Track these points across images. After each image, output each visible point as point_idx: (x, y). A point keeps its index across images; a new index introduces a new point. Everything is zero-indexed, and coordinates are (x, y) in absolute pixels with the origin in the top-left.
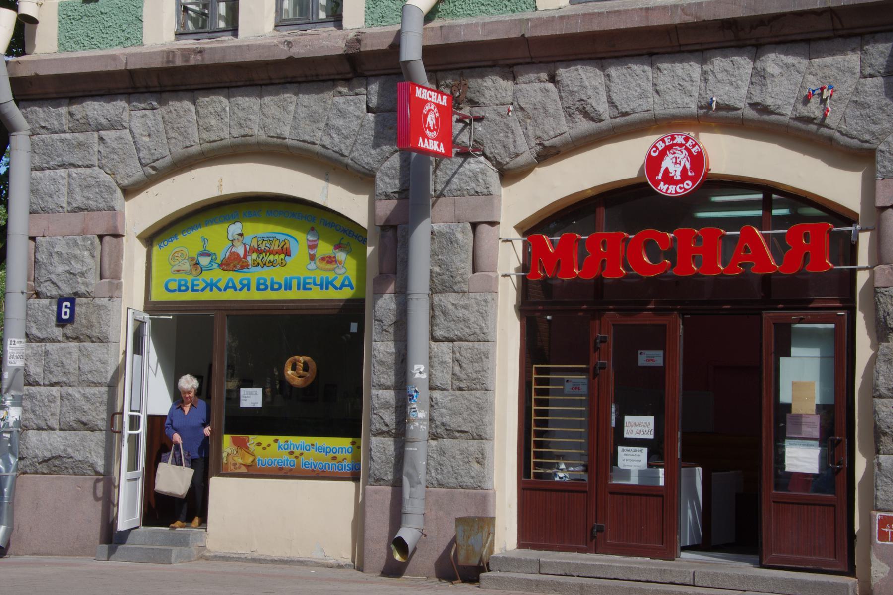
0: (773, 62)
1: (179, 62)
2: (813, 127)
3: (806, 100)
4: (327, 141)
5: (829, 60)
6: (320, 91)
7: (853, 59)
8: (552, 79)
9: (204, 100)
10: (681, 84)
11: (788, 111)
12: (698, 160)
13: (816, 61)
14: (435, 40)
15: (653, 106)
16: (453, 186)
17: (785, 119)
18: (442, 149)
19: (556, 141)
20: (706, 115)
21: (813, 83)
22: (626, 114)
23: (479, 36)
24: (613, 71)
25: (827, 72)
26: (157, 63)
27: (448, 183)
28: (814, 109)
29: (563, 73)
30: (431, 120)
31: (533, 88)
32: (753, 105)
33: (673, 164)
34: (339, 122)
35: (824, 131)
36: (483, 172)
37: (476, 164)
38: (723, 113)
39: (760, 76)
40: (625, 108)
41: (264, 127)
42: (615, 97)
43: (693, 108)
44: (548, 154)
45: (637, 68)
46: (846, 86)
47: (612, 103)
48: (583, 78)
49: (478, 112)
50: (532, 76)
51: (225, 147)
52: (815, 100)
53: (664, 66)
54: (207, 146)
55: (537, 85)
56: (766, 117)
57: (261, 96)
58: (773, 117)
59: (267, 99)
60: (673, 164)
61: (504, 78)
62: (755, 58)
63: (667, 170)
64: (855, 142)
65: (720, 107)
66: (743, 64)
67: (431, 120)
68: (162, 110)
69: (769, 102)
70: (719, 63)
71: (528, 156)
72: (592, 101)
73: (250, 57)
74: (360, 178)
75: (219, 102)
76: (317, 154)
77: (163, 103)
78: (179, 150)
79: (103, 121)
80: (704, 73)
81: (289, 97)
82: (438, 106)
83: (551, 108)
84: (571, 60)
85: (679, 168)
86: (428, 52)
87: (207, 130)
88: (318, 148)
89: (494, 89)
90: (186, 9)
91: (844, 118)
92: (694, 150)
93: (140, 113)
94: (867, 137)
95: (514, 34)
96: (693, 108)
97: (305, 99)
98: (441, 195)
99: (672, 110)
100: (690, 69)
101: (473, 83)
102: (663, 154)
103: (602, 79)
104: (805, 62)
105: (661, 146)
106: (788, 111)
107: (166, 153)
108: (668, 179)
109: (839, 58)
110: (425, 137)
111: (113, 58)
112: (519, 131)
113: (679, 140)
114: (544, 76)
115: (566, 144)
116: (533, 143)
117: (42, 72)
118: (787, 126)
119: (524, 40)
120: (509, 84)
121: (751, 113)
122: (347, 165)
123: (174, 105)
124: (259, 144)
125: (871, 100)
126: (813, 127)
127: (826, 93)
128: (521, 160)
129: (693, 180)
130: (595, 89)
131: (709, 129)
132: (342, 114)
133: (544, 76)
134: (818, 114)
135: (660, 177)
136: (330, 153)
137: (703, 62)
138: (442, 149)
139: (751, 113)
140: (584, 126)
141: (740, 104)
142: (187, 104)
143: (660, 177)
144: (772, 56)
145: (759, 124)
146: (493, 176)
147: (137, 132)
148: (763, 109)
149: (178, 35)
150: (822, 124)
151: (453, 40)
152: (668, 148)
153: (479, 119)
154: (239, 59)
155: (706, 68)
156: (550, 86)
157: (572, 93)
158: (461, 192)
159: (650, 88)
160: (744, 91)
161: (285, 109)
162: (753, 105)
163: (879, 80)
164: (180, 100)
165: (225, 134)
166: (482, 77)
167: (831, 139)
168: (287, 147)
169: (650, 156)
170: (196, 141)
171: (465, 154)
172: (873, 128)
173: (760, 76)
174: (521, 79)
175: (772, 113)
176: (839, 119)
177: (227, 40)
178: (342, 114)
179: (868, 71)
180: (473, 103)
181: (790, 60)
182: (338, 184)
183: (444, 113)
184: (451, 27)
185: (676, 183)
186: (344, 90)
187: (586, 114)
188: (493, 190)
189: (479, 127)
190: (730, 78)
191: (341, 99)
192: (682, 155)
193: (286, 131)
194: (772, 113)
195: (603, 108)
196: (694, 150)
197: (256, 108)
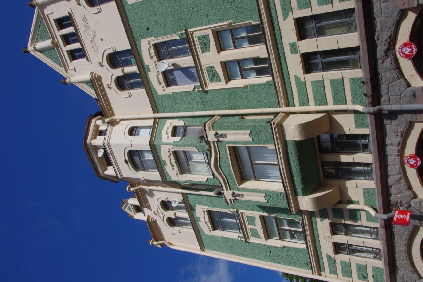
0: (388, 142)
1: (387, 263)
2: (404, 134)
3: (397, 135)
4: (406, 234)
5: (387, 131)
6: (394, 235)
7: (387, 127)
8: (391, 186)
9: (396, 258)
10: (393, 160)
11: (400, 139)
12: (411, 157)
13: (388, 133)
14: (382, 211)
15: (398, 167)
16: (418, 209)
17: (402, 139)
18: (409, 214)
19: (407, 186)
20: (400, 155)
21: (393, 134)
22: (400, 172)
23: (381, 202)
24: (389, 174)
25: (390, 131)
26: (388, 267)
27: (417, 210)
28: (399, 134)
29: (390, 184)
30: (402, 217)
31: (393, 190)
32: (398, 146)
33: (412, 162)
34: (402, 231)
35: (405, 131)
36: (414, 202)
37: (412, 203)
38: (400, 152)
39: (391, 144)
40: (398, 172)
41: (403, 247)
42: (396, 174)
43: (398, 158)
44: (410, 188)
45: (389, 169)
46: (393, 127)
47: (397, 174)
48: (391, 180)
49: (399, 202)
50: (390, 191)
51: (408, 256)
52: (397, 134)
53: (388, 164)
54: (408, 259)
55: (393, 189)
56: (401, 143)
57: (395, 247)
58: (401, 142)
59: (396, 245)
60: (412, 162)
61: (391, 196)
62: (387, 145)
63: (409, 52)
64: (407, 125)
65: (398, 152)
66: (388, 148)
67: (402, 217)
68: (399, 267)
69: (397, 143)
70: (388, 153)
71: (410, 192)
72: (397, 179)
73: (386, 249)
74: (411, 126)
75: (397, 255)
76: (410, 237)
77: (397, 267)
78: (409, 265)
79: (402, 280)
80: (390, 155)
81: (395, 241)
82: (398, 214)
83: (398, 187)
84: (387, 183)
85: (408, 49)
86: (385, 213)
87: (404, 259)
88: (408, 237)
89: (393, 198)
90: (374, 257)
91: (402, 128)
92: (403, 46)
93: (400, 272)
94: (406, 123)
95: (381, 195)
96: (398, 158)
97: (396, 238)
98: (421, 212)
99: (399, 162)
100: (389, 158)
101: (392, 203)
102: (410, 164)
103: (391, 176)
104: (388, 136)
105: (408, 164)
106: (400, 139)
107: (410, 268)
108: (412, 52)
109: (387, 129)
110: (406, 219)
111: (386, 276)
112: (404, 194)
113: (406, 161)
114: (390, 188)
115: (407, 184)
116: (407, 191)
117: (380, 191)
118: (403, 139)
119: (382, 193)
120: (392, 196)
121: (400, 146)
122: (413, 231)
123: (397, 265)
124: (407, 248)
125: (397, 123)
126: (404, 134)
127: (395, 132)
128: (411, 194)
129: (416, 158)
130: (394, 178)
131: (404, 154)
132: (399, 230)
133: (390, 188)
134: (400, 133)
135: (411, 54)
136: (409, 234)
137: (387, 156)
138: (409, 214)
139: (400, 146)
140: (403, 180)
141: (398, 148)
142: (397, 262)
143: (411, 54)
144: (386, 142)
145: (403, 145)
146: (415, 200)
147: (404, 273)
148: (399, 144)
149: (380, 260)
150: (403, 132)
151: (382, 207)
152: (408, 163)
153: (401, 202)
154: (386, 251)
155: (389, 155)
156: (393, 187)
157: (394, 183)
158: (420, 207)
159: (394, 166)
160: (394, 148)
161: (398, 242)
162: (398, 146)
163: (392, 121)
164: (396, 263)
165: (405, 255)
166: (390, 201)
167: (407, 130)
168: (408, 243)
169: (405, 58)
170: (406, 261)
171: (410, 206)
172: (404, 122)
173: (391, 144)
174: (391, 193)
175: (400, 142)
176: (402, 129)
177: (373, 165)
178: (399, 230)
179: (390, 123)
180: (397, 203)
181: (387, 139)
182: (417, 233)
183: (400, 212)
184: (379, 207)
185: (413, 49)
186: (394, 229)
187: (400, 180)
188: (419, 200)
189: (403, 202)
190: (392, 151)
191: (396, 230)
192: (410, 160)
193: (404, 243)
194: (400, 142)
195: (398, 176)
196: (403, 46)
197: (398, 248)
